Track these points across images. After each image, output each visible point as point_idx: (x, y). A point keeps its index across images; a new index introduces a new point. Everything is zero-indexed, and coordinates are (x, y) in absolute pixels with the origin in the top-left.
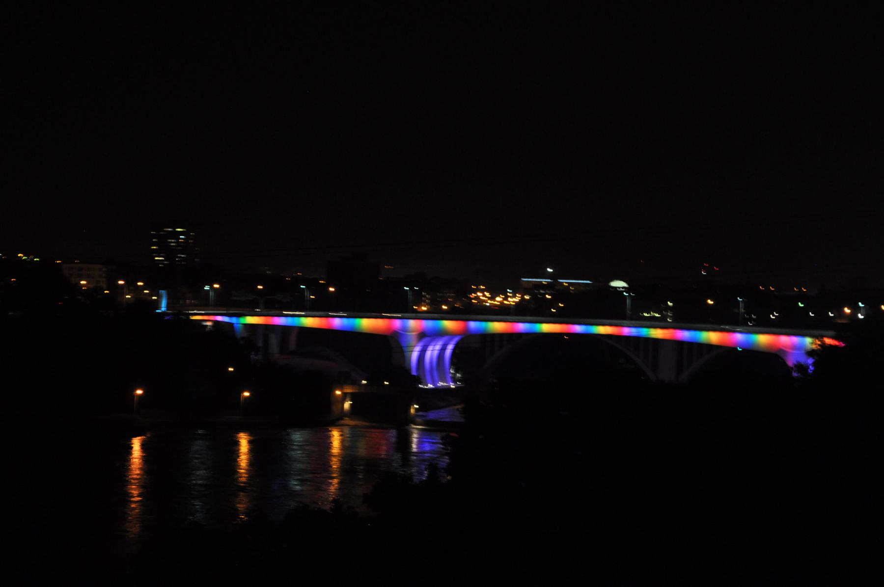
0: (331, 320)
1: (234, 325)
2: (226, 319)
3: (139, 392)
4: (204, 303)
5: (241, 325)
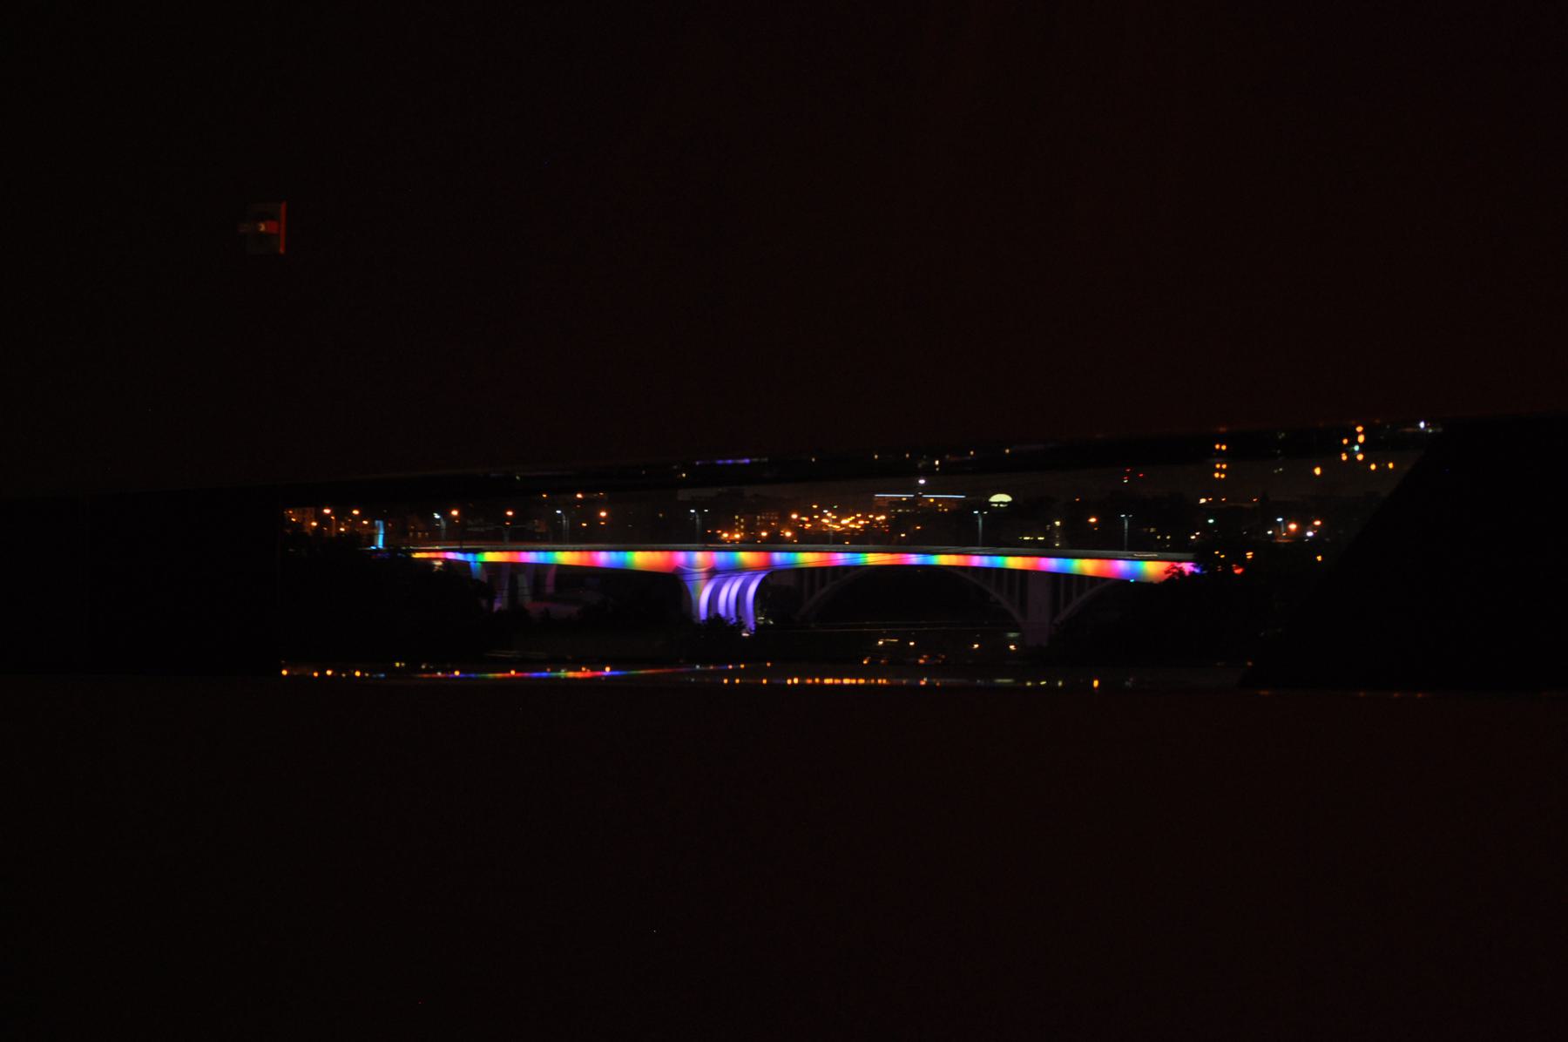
0: (594, 554)
1: (472, 564)
2: (460, 556)
4: (434, 537)
5: (479, 564)
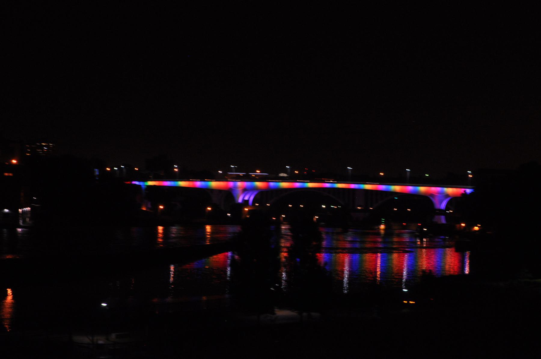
3: (161, 207)
